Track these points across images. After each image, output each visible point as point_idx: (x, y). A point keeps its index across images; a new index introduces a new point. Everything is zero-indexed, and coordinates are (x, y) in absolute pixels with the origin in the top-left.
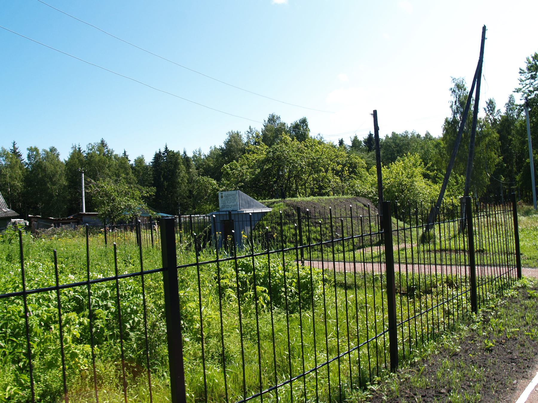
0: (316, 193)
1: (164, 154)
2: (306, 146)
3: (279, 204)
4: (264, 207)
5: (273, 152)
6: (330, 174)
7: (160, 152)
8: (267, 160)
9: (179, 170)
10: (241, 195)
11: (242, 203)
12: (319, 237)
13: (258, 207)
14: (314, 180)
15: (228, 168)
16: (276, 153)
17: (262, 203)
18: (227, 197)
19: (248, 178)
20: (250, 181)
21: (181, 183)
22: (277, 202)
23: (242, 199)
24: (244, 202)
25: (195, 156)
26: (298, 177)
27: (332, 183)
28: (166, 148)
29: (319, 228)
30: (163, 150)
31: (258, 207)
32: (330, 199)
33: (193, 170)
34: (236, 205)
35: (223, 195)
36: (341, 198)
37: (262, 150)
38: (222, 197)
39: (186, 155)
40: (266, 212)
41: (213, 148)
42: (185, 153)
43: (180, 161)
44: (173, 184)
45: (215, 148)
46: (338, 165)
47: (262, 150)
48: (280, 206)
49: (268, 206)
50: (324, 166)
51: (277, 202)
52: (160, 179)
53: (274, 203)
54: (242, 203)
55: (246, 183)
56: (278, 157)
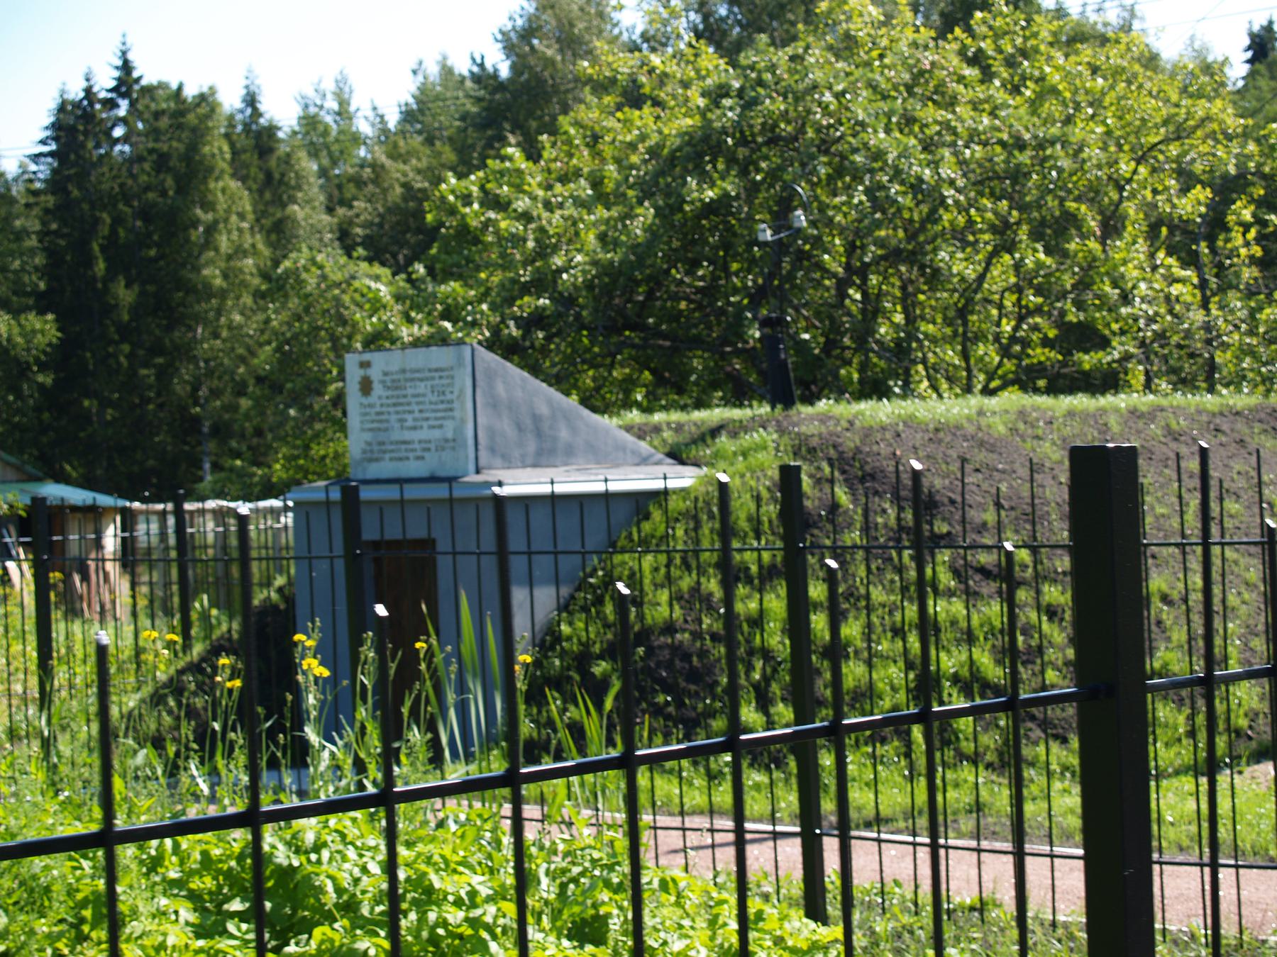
0: (1038, 370)
1: (110, 104)
2: (977, 60)
3: (747, 440)
4: (644, 461)
5: (741, 93)
6: (1131, 253)
7: (88, 91)
8: (701, 150)
9: (208, 206)
10: (491, 375)
11: (492, 432)
12: (994, 672)
13: (602, 455)
14: (1024, 280)
15: (467, 199)
16: (755, 102)
17: (641, 432)
18: (395, 386)
19: (575, 265)
20: (589, 286)
21: (223, 294)
22: (735, 430)
23: (494, 405)
24: (506, 426)
25: (310, 122)
26: (912, 254)
27: (1139, 307)
28: (126, 67)
29: (994, 610)
30: (105, 81)
31: (612, 457)
32: (1103, 411)
33: (308, 211)
34: (454, 443)
35: (375, 373)
36: (1176, 411)
37: (686, 85)
38: (366, 387)
39: (257, 114)
40: (641, 502)
41: (433, 70)
42: (251, 100)
43: (217, 149)
44: (171, 293)
45: (447, 71)
46: (1184, 190)
47: (686, 85)
48: (748, 448)
49: (677, 455)
50: (1092, 195)
51: (735, 430)
52: (89, 262)
53: (715, 432)
54: (492, 432)
55: (566, 301)
56: (770, 128)
